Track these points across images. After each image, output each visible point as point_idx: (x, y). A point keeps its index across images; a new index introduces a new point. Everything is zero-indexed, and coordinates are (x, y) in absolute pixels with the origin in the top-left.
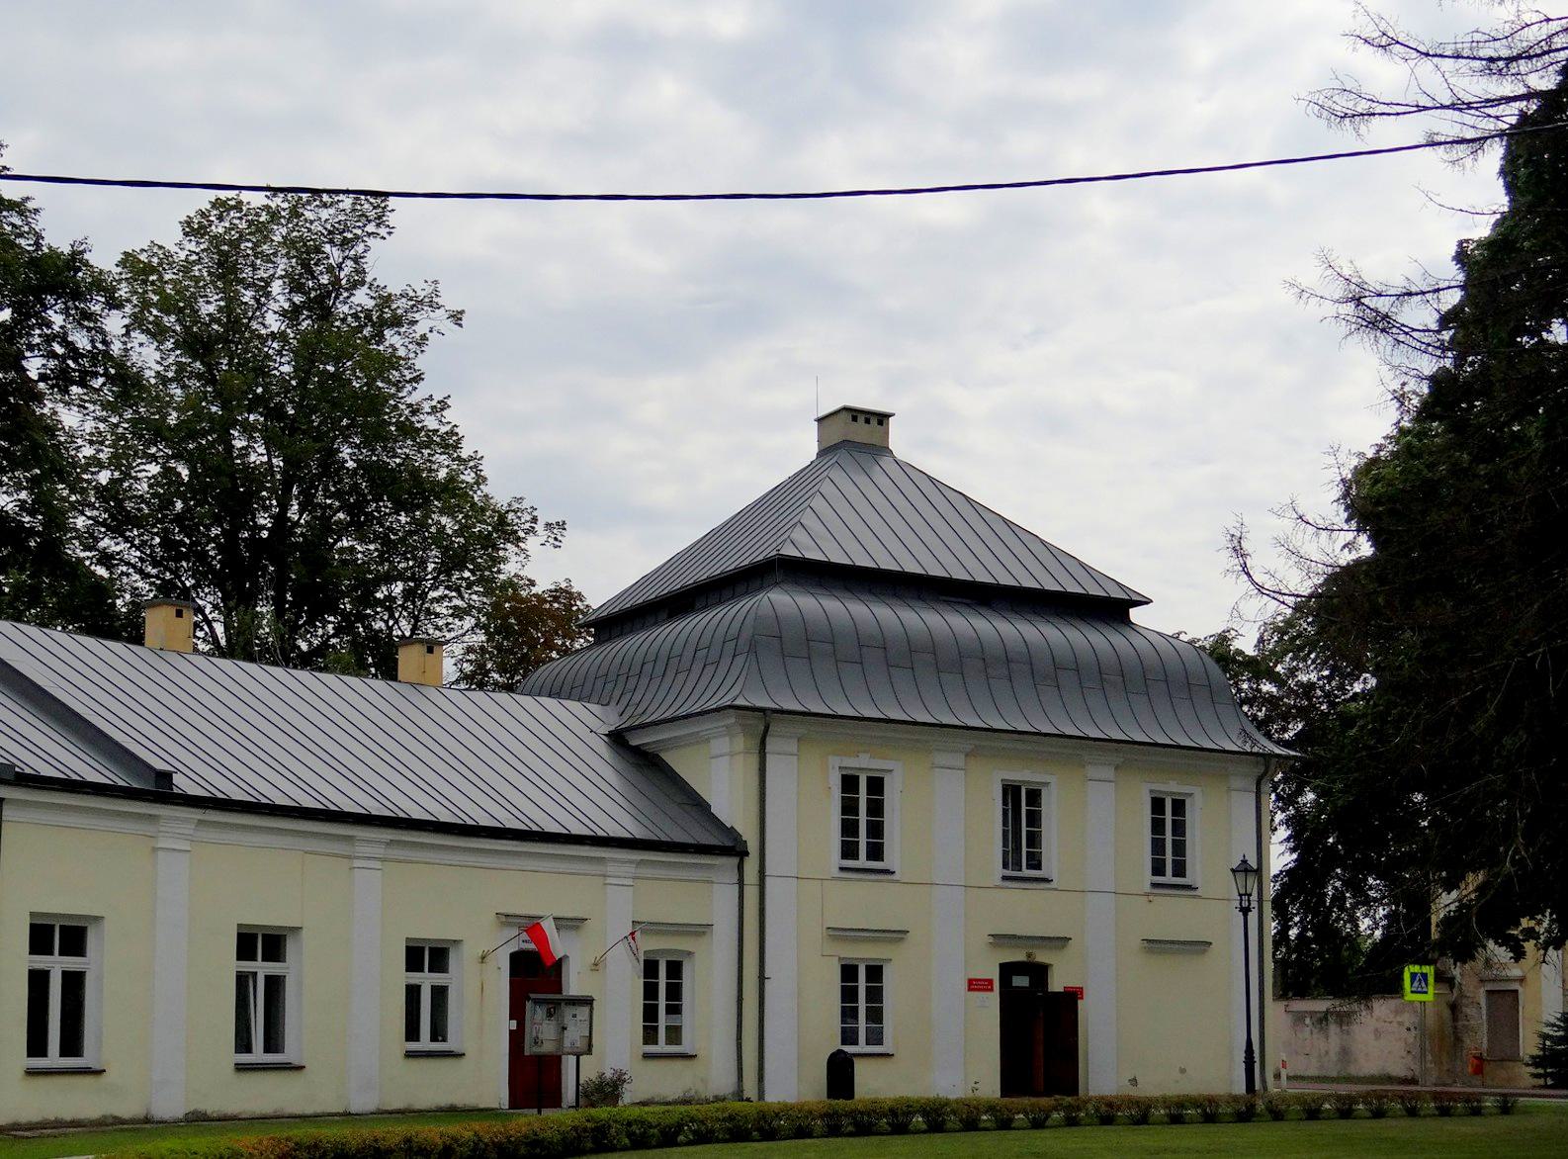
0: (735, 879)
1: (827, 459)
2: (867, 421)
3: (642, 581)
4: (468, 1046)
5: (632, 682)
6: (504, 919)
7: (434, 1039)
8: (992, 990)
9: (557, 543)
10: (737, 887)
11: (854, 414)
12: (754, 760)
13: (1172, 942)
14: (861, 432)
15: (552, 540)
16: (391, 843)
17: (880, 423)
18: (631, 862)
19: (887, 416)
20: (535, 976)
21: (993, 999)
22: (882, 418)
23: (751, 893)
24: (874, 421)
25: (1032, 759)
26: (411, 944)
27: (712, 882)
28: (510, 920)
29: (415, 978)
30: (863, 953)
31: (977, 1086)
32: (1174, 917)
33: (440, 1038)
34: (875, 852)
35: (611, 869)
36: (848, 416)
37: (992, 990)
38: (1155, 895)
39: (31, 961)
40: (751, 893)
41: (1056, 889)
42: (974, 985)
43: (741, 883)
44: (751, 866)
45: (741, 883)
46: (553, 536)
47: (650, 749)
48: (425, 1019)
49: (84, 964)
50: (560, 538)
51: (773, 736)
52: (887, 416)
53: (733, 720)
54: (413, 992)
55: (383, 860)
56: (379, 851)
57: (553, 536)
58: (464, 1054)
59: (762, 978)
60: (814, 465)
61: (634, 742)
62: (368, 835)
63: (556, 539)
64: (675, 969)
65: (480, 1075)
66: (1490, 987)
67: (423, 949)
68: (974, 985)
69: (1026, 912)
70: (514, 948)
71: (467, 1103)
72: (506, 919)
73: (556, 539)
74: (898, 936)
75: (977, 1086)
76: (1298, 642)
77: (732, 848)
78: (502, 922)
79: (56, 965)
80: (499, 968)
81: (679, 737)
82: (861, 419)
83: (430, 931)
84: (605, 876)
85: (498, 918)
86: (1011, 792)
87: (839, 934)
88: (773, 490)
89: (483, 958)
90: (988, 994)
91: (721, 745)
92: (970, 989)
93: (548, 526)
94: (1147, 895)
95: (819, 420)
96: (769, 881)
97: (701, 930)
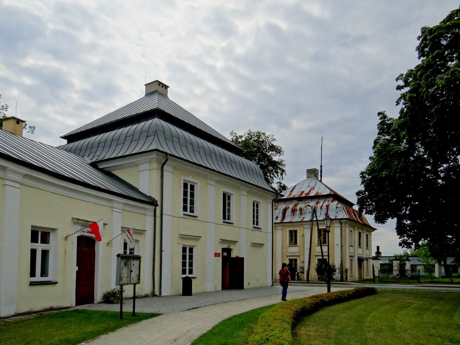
0: (153, 215)
1: (147, 97)
2: (162, 87)
3: (84, 126)
4: (59, 279)
5: (94, 150)
6: (76, 221)
7: (42, 275)
8: (220, 256)
9: (32, 132)
10: (153, 217)
11: (160, 83)
12: (159, 172)
13: (257, 244)
14: (161, 89)
15: (31, 131)
16: (26, 176)
17: (166, 88)
18: (122, 203)
19: (168, 87)
20: (86, 248)
21: (220, 259)
22: (166, 87)
23: (158, 220)
24: (164, 87)
25: (233, 187)
26: (33, 229)
27: (146, 215)
28: (79, 221)
29: (35, 246)
30: (189, 243)
31: (216, 287)
32: (257, 237)
33: (44, 275)
34: (192, 211)
35: (115, 205)
36: (157, 83)
37: (220, 256)
38: (254, 230)
39: (31, 246)
40: (158, 220)
41: (234, 226)
42: (217, 255)
43: (155, 216)
44: (158, 209)
45: (155, 216)
46: (31, 130)
47: (107, 170)
48: (39, 265)
49: (49, 247)
50: (33, 131)
51: (167, 165)
52: (168, 87)
53: (155, 156)
54: (33, 252)
55: (21, 184)
56: (20, 179)
57: (31, 130)
58: (57, 283)
59: (161, 251)
60: (143, 98)
61: (100, 167)
62: (18, 169)
63: (32, 131)
64: (191, 250)
65: (63, 293)
66: (290, 258)
67: (38, 232)
68: (217, 255)
69: (228, 233)
70: (79, 234)
71: (57, 305)
72: (77, 221)
73: (32, 131)
74: (197, 238)
75: (216, 287)
76: (415, 138)
77: (152, 202)
78: (74, 222)
79: (40, 247)
80: (73, 243)
81: (124, 164)
82: (161, 85)
83: (43, 223)
84: (112, 208)
85: (73, 220)
86: (224, 195)
87: (183, 237)
88: (118, 110)
89: (66, 238)
90: (218, 258)
91: (147, 166)
92: (215, 256)
93: (30, 127)
94: (252, 230)
95: (146, 85)
96: (164, 216)
97: (141, 232)
